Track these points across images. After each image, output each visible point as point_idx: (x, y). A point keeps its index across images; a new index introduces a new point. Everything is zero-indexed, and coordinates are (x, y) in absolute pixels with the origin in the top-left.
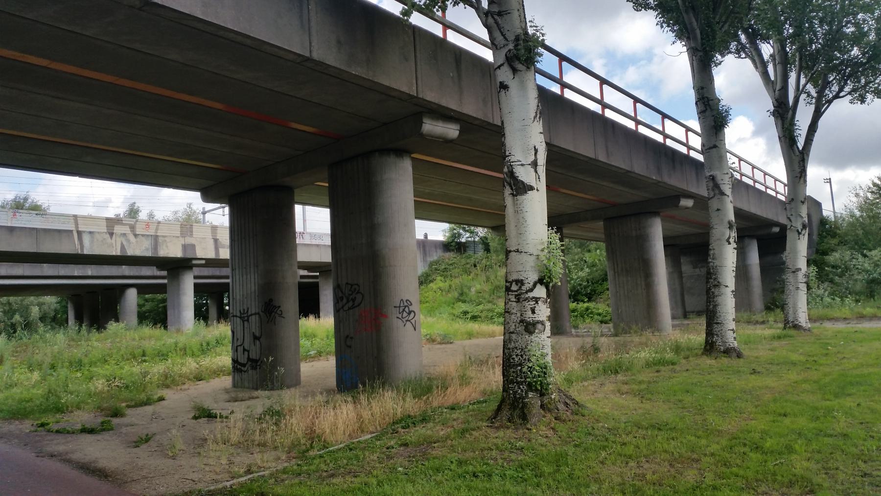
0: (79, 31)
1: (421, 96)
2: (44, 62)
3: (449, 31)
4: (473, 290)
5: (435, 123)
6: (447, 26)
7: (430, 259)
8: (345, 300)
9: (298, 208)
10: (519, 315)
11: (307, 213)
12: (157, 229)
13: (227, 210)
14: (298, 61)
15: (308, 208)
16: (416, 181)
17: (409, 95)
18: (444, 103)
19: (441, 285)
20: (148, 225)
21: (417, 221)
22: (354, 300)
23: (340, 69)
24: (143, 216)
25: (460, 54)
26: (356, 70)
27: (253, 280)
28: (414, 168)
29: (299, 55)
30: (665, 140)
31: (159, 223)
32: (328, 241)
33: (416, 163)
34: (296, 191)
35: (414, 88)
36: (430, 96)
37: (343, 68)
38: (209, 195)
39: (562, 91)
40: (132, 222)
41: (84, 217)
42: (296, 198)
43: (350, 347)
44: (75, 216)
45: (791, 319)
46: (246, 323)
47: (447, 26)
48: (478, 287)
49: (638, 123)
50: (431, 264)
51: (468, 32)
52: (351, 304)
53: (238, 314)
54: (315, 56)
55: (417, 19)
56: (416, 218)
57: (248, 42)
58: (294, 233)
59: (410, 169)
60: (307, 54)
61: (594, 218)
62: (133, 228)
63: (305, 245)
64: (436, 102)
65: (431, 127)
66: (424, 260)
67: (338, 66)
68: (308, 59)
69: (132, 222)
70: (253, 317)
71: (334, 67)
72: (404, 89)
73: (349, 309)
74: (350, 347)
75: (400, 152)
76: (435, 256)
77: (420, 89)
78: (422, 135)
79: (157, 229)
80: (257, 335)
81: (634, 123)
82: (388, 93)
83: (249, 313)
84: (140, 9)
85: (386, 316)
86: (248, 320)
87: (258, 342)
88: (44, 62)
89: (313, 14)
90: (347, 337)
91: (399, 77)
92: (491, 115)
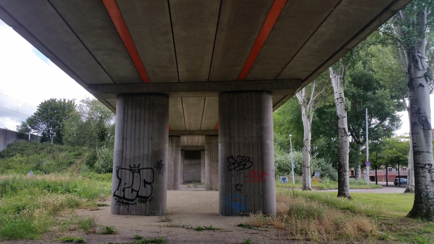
4: (44, 163)
7: (8, 142)
8: (236, 165)
10: (430, 178)
19: (20, 158)
22: (244, 165)
27: (146, 146)
43: (240, 190)
45: (307, 186)
46: (136, 174)
48: (48, 162)
50: (9, 146)
52: (242, 167)
53: (129, 168)
61: (202, 134)
66: (5, 143)
70: (145, 171)
73: (240, 169)
74: (240, 190)
76: (11, 141)
80: (149, 180)
83: (141, 167)
85: (269, 175)
86: (139, 172)
87: (149, 186)
90: (238, 184)
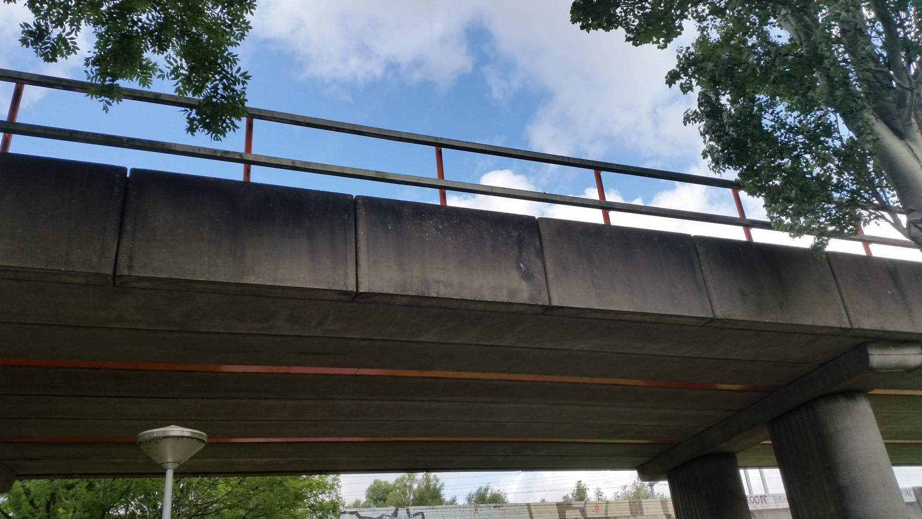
0: (311, 334)
1: (857, 327)
2: (415, 373)
3: (612, 214)
5: (886, 352)
6: (867, 241)
9: (742, 471)
11: (766, 476)
12: (607, 510)
13: (666, 482)
14: (702, 323)
15: (765, 471)
16: (881, 423)
17: (841, 328)
18: (889, 327)
20: (597, 506)
21: (895, 469)
23: (751, 321)
24: (591, 495)
25: (893, 269)
26: (768, 318)
28: (873, 406)
29: (702, 318)
30: (867, 249)
31: (607, 502)
32: (786, 505)
33: (878, 404)
34: (739, 456)
35: (846, 320)
36: (869, 323)
37: (754, 319)
38: (648, 473)
39: (748, 234)
40: (580, 504)
41: (536, 505)
42: (739, 464)
44: (528, 505)
47: (867, 241)
49: (606, 207)
51: (164, 144)
54: (719, 314)
55: (835, 246)
56: (894, 464)
57: (647, 318)
58: (744, 498)
59: (870, 411)
60: (711, 316)
62: (583, 511)
63: (770, 510)
64: (879, 328)
65: (879, 357)
67: (748, 319)
68: (712, 320)
69: (580, 504)
71: (743, 321)
72: (834, 323)
75: (851, 394)
77: (853, 319)
78: (872, 370)
79: (607, 510)
81: (860, 244)
82: (815, 333)
84: (543, 314)
88: (415, 373)
89: (707, 273)
91: (824, 313)
92: (544, 293)
